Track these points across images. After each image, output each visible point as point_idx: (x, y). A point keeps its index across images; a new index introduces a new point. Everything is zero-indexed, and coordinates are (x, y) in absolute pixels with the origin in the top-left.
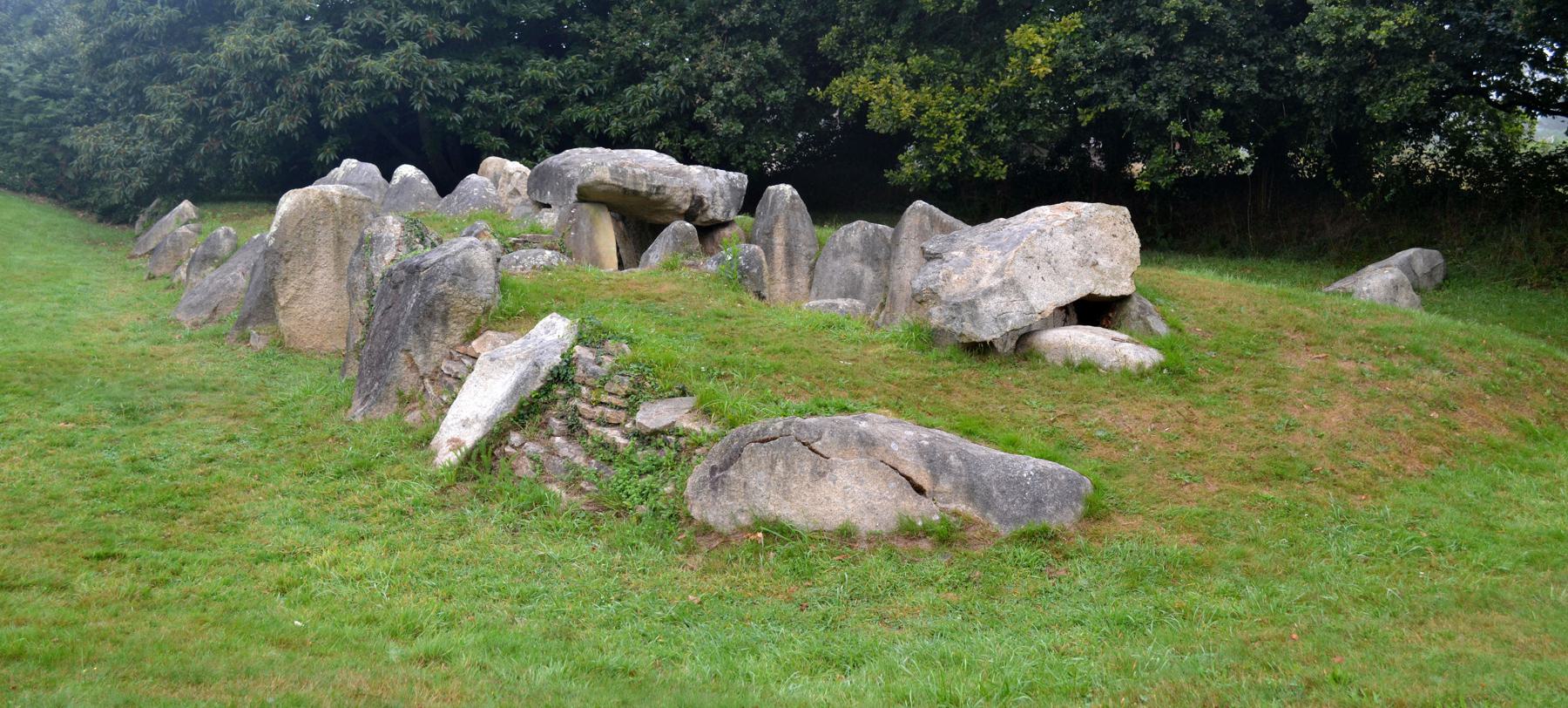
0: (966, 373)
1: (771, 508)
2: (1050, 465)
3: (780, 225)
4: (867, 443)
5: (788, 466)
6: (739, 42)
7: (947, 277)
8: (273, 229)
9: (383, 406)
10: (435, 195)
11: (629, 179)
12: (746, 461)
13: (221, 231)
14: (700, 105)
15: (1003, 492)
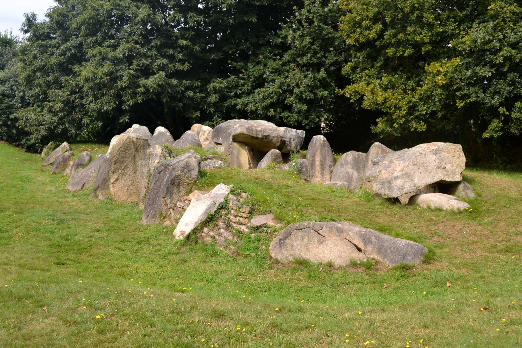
0: (386, 209)
1: (302, 254)
2: (412, 242)
3: (318, 153)
4: (340, 231)
5: (309, 239)
6: (307, 70)
7: (380, 172)
8: (109, 151)
9: (154, 219)
10: (172, 140)
11: (254, 132)
12: (293, 237)
13: (85, 153)
14: (289, 97)
15: (392, 251)
